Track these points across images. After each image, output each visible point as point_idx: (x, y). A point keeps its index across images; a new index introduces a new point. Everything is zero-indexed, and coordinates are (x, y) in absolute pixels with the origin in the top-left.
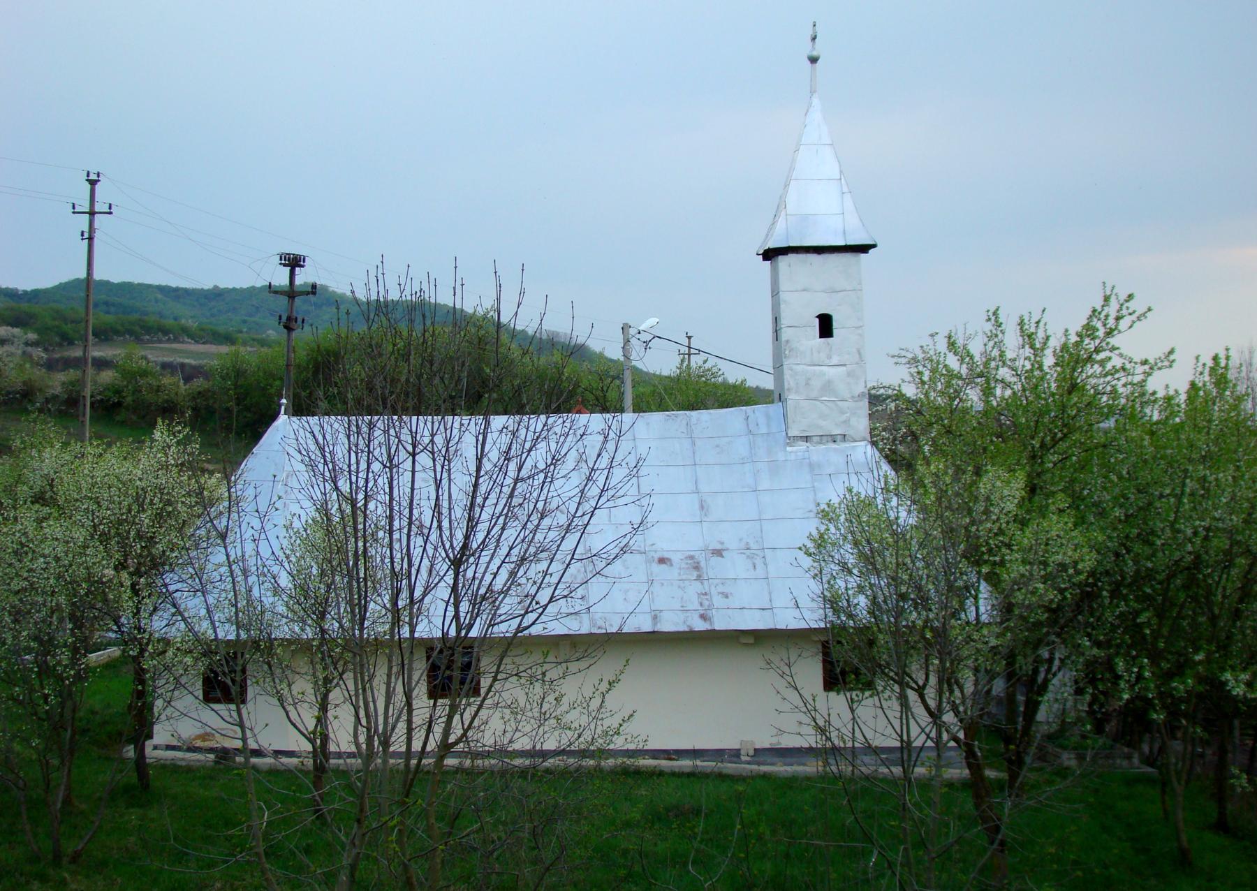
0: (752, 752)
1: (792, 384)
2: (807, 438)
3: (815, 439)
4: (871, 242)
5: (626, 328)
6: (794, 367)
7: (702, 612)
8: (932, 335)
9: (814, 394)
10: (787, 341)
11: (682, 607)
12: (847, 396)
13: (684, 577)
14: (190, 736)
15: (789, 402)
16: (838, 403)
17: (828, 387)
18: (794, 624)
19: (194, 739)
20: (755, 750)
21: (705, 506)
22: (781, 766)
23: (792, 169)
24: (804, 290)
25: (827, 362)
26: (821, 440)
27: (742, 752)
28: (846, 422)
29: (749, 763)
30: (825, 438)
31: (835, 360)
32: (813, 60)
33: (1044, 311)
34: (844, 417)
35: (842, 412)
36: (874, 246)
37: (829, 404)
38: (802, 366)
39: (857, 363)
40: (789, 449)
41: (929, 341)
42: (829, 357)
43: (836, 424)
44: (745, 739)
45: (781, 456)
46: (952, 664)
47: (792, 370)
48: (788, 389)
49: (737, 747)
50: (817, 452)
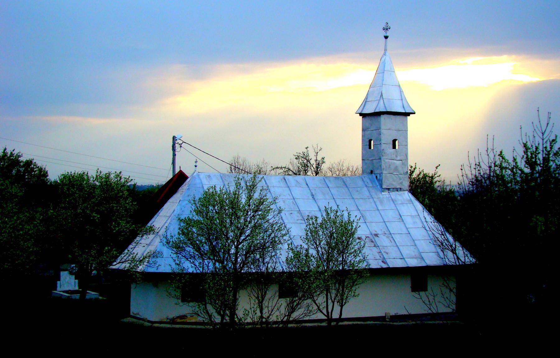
0: (389, 317)
1: (384, 167)
2: (389, 189)
3: (391, 190)
4: (414, 112)
5: (174, 138)
6: (385, 160)
7: (382, 260)
8: (306, 148)
9: (391, 172)
10: (383, 150)
11: (374, 258)
12: (402, 172)
13: (370, 245)
14: (173, 318)
15: (383, 174)
16: (399, 175)
17: (396, 169)
18: (399, 264)
19: (176, 319)
20: (391, 316)
21: (364, 216)
22: (399, 322)
23: (202, 183)
24: (389, 129)
25: (396, 158)
26: (393, 190)
27: (387, 317)
28: (401, 183)
29: (388, 321)
30: (394, 189)
31: (398, 158)
32: (386, 37)
33: (488, 135)
34: (401, 181)
35: (400, 179)
36: (414, 113)
37: (396, 176)
38: (388, 160)
39: (405, 160)
40: (383, 193)
41: (305, 150)
42: (396, 156)
43: (398, 184)
44: (387, 312)
45: (381, 196)
46: (214, 238)
47: (384, 161)
48: (383, 169)
49: (384, 315)
50: (394, 195)
